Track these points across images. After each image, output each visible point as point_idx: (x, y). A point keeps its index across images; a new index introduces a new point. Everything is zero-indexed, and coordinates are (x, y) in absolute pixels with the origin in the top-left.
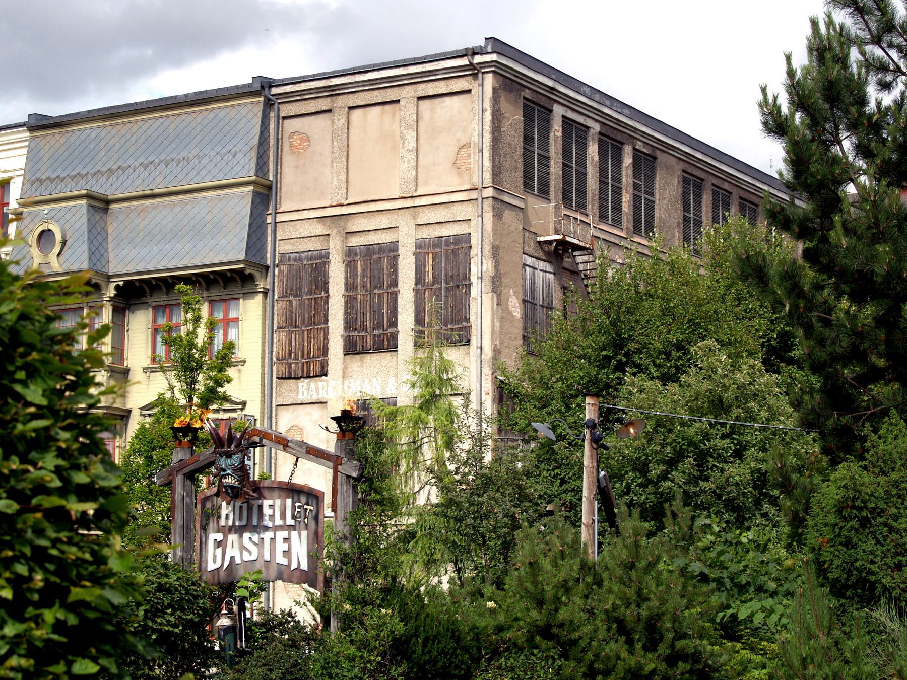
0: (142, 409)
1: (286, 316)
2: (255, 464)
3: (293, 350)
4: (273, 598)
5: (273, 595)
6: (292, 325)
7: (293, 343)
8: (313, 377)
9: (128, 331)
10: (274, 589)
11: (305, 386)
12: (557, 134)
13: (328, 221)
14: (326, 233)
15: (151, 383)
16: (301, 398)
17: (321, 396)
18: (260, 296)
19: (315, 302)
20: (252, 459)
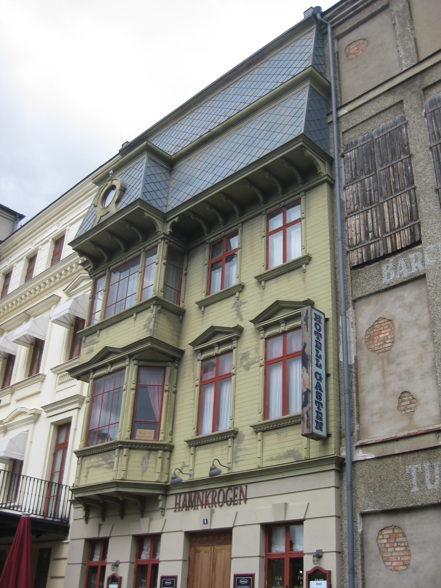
0: (254, 321)
1: (358, 198)
2: (328, 375)
3: (371, 229)
4: (363, 571)
5: (363, 565)
6: (366, 204)
7: (370, 222)
8: (402, 250)
9: (186, 274)
10: (363, 557)
11: (391, 265)
12: (417, 182)
13: (399, 90)
14: (399, 100)
15: (205, 317)
16: (386, 281)
17: (414, 270)
18: (325, 188)
19: (393, 169)
20: (324, 427)
